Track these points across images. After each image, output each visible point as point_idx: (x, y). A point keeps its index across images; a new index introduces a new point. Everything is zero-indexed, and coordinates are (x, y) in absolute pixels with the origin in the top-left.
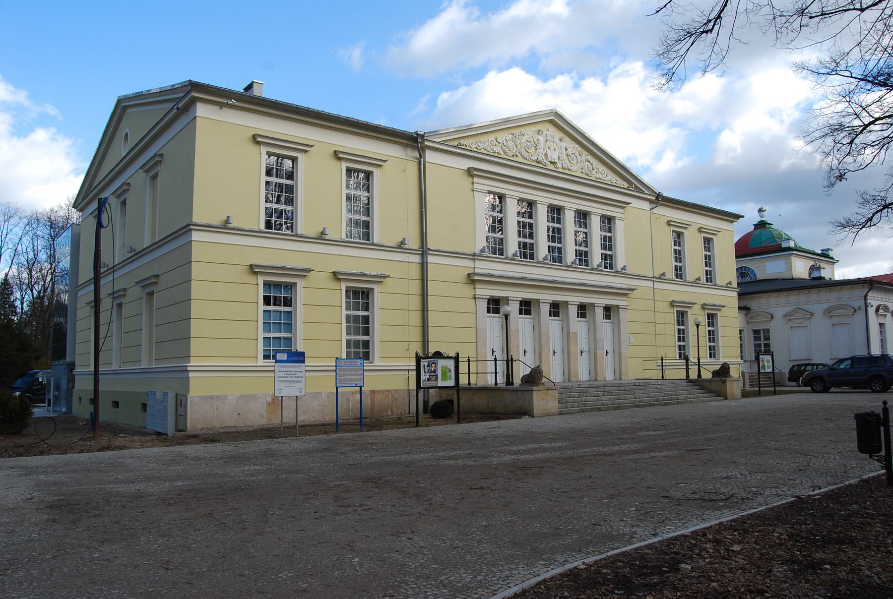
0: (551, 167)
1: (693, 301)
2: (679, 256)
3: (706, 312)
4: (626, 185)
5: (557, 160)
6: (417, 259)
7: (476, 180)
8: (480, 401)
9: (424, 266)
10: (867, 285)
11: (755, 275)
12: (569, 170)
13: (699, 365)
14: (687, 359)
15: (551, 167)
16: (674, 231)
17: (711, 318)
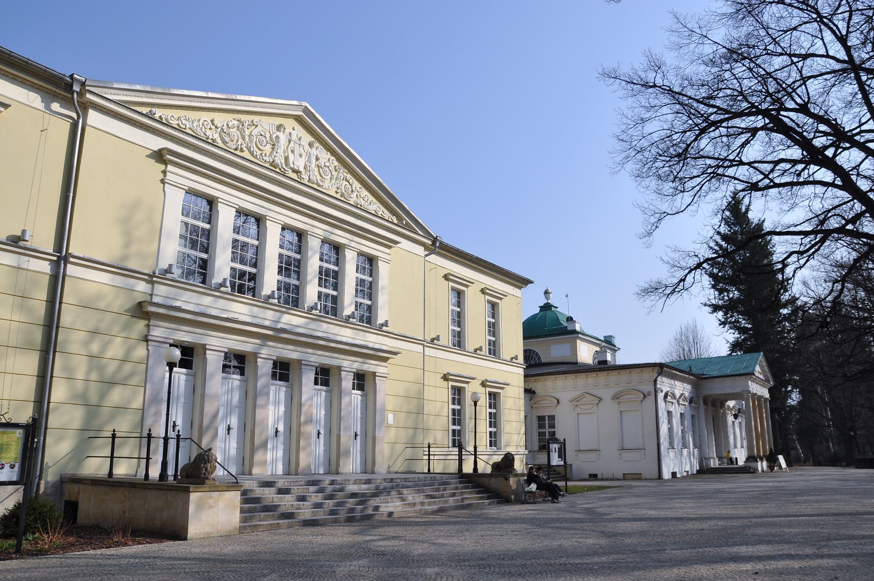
0: (294, 176)
1: (508, 382)
2: (459, 319)
3: (488, 389)
4: (395, 221)
5: (302, 169)
6: (45, 267)
7: (170, 168)
8: (113, 506)
9: (56, 281)
10: (656, 369)
11: (539, 358)
12: (319, 185)
13: (475, 455)
14: (461, 447)
15: (294, 176)
16: (453, 289)
17: (494, 397)
